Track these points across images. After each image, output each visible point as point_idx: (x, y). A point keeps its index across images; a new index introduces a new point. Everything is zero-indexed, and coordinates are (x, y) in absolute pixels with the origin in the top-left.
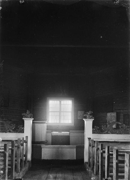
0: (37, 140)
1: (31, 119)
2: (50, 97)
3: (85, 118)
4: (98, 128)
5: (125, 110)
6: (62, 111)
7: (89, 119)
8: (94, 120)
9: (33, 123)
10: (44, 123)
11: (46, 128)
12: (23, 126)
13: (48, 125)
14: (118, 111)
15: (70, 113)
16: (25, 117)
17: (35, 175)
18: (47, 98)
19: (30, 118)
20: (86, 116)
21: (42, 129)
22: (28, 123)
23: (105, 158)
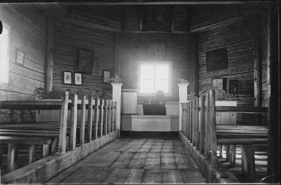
0: (125, 112)
1: (120, 84)
2: (140, 60)
3: (180, 82)
4: (194, 94)
5: (232, 76)
6: (217, 123)
7: (183, 83)
8: (188, 84)
9: (122, 91)
10: (135, 92)
11: (136, 99)
12: (112, 93)
13: (139, 95)
14: (225, 77)
15: (168, 80)
16: (114, 82)
17: (124, 140)
18: (171, 62)
19: (120, 83)
20: (181, 81)
21: (132, 97)
22: (117, 88)
23: (199, 127)
